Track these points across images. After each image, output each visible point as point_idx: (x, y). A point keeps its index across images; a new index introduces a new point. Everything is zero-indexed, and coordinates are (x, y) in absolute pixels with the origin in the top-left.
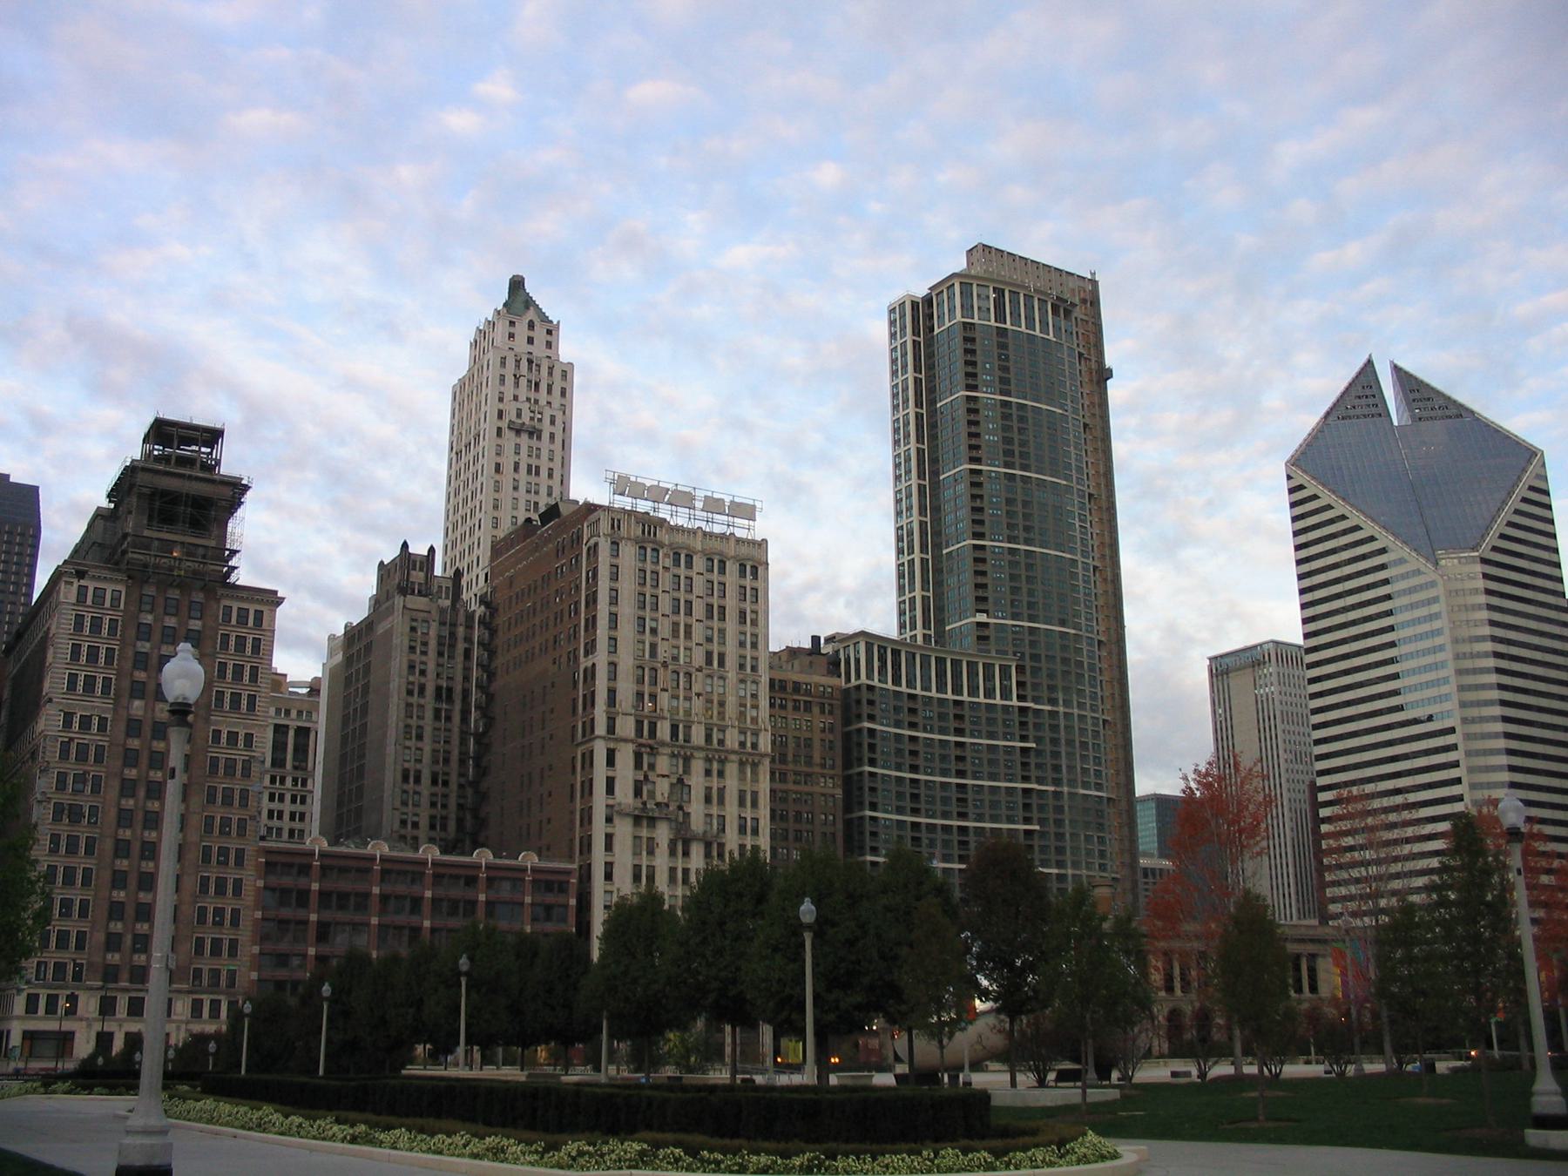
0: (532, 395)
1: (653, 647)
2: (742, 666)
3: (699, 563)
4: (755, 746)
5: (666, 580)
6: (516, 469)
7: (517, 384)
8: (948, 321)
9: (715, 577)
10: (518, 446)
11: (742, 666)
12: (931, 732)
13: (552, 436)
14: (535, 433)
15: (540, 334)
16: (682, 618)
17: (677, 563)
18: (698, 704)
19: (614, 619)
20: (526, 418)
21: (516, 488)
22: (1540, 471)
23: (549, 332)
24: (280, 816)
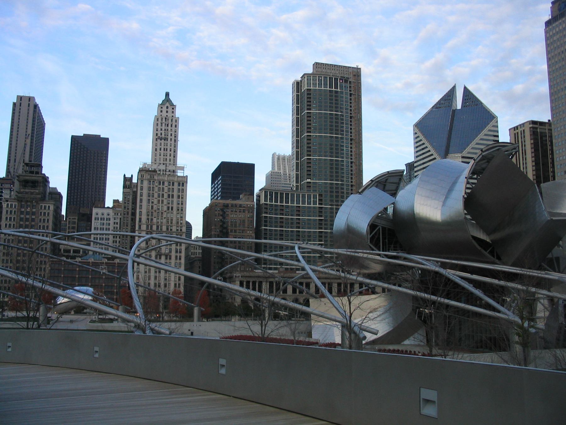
0: (166, 128)
1: (152, 207)
2: (178, 210)
3: (166, 184)
4: (181, 230)
5: (156, 189)
6: (160, 150)
7: (162, 125)
8: (305, 87)
9: (171, 187)
10: (161, 143)
11: (178, 210)
12: (288, 215)
13: (171, 139)
14: (166, 139)
15: (170, 110)
16: (161, 199)
17: (160, 184)
18: (164, 221)
19: (141, 200)
20: (163, 136)
21: (160, 155)
22: (495, 124)
23: (173, 109)
24: (116, 242)
